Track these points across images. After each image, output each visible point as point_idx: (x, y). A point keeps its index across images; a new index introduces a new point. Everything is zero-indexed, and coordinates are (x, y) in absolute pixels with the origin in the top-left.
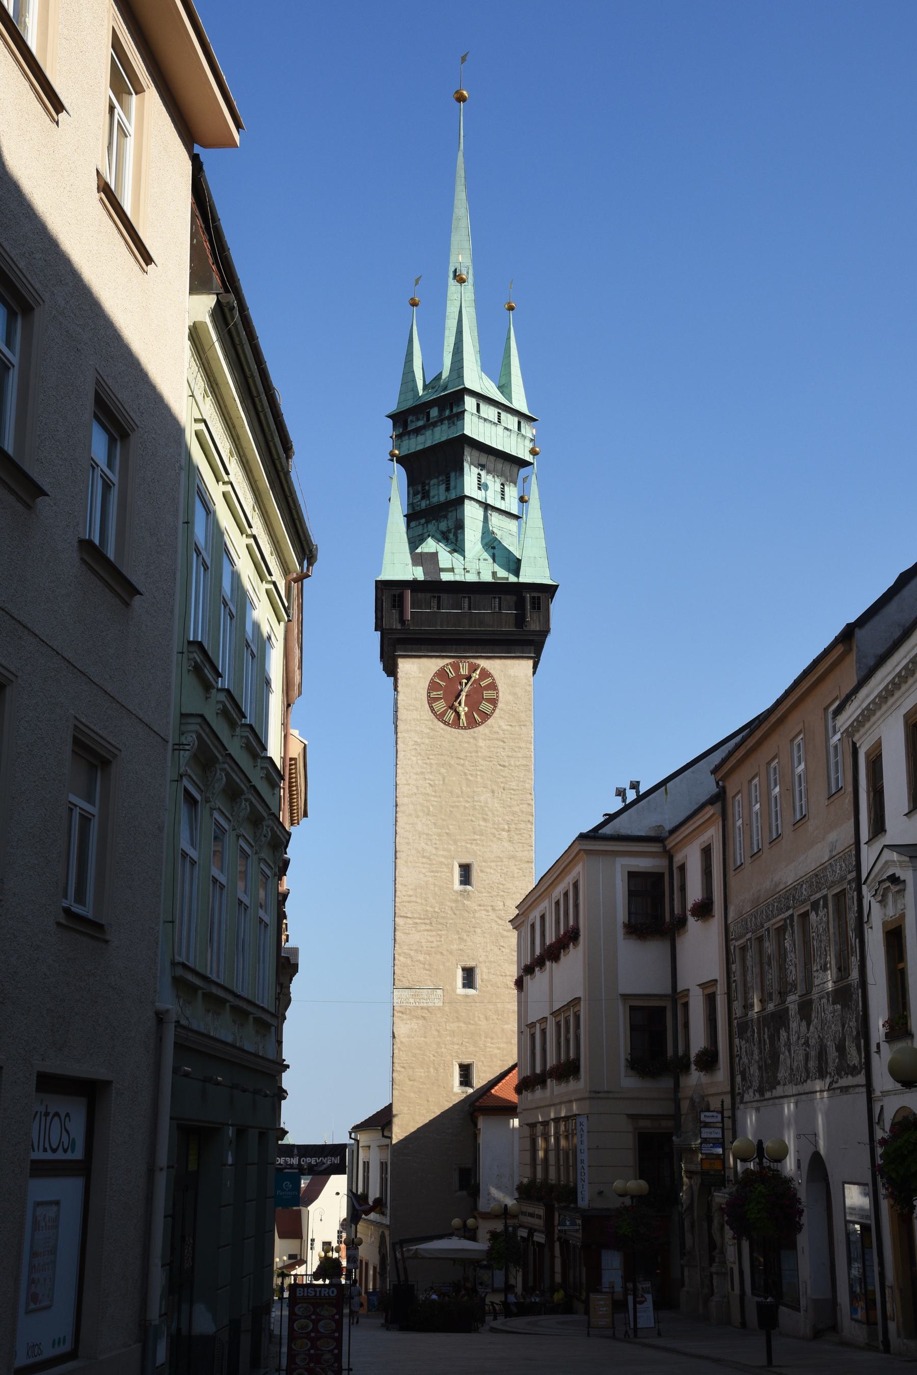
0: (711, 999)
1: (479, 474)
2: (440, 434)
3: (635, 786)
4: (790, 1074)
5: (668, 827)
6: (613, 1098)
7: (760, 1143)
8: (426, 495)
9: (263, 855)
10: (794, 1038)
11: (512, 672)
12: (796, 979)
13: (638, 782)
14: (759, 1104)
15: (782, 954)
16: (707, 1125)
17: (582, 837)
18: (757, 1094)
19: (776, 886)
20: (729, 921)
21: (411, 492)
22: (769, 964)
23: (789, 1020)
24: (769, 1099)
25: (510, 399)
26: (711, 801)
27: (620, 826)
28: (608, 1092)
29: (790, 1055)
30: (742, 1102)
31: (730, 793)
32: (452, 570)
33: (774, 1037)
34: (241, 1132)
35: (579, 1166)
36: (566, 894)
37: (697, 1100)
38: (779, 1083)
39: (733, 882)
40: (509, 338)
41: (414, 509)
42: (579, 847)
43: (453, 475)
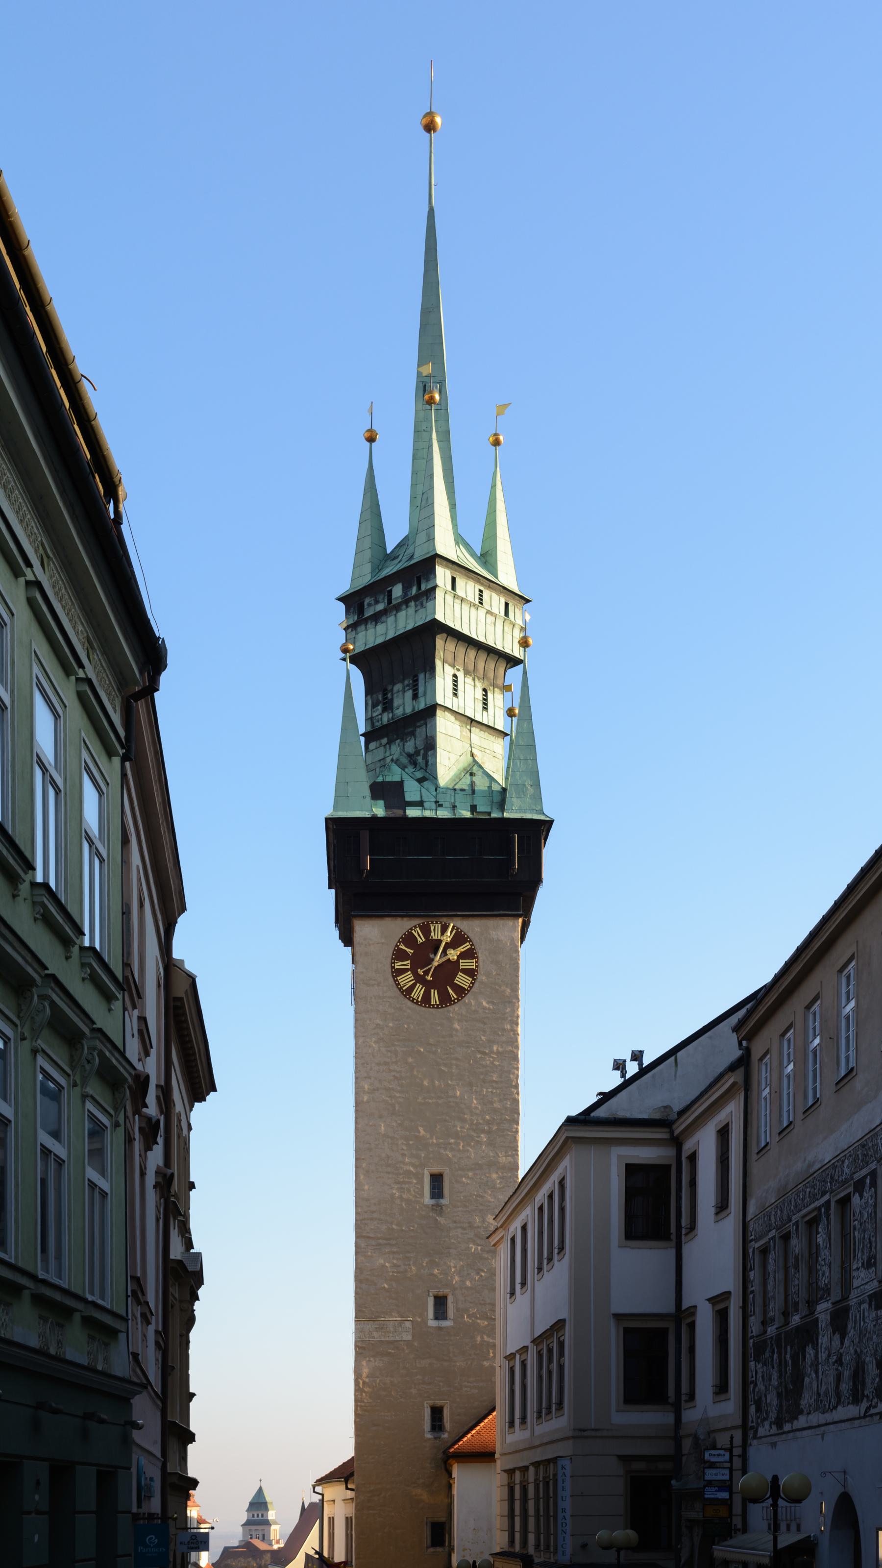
0: (722, 1316)
1: (455, 676)
2: (406, 621)
3: (637, 1056)
4: (816, 1401)
5: (677, 1107)
6: (602, 1437)
7: (775, 1479)
8: (388, 706)
9: (89, 1090)
10: (823, 1356)
11: (494, 934)
12: (829, 1282)
13: (641, 1052)
14: (775, 1439)
15: (813, 1253)
16: (712, 1465)
17: (570, 1121)
18: (774, 1427)
19: (810, 1166)
20: (749, 1218)
21: (370, 702)
22: (796, 1267)
23: (818, 1335)
24: (789, 1432)
25: (495, 573)
26: (732, 1068)
27: (618, 1108)
28: (596, 1430)
29: (817, 1377)
30: (755, 1437)
31: (756, 1054)
32: (420, 804)
33: (798, 1357)
34: (61, 1473)
35: (560, 1515)
36: (551, 1196)
37: (702, 1437)
38: (801, 1412)
39: (756, 1169)
40: (494, 486)
41: (373, 724)
42: (567, 1134)
43: (421, 676)
